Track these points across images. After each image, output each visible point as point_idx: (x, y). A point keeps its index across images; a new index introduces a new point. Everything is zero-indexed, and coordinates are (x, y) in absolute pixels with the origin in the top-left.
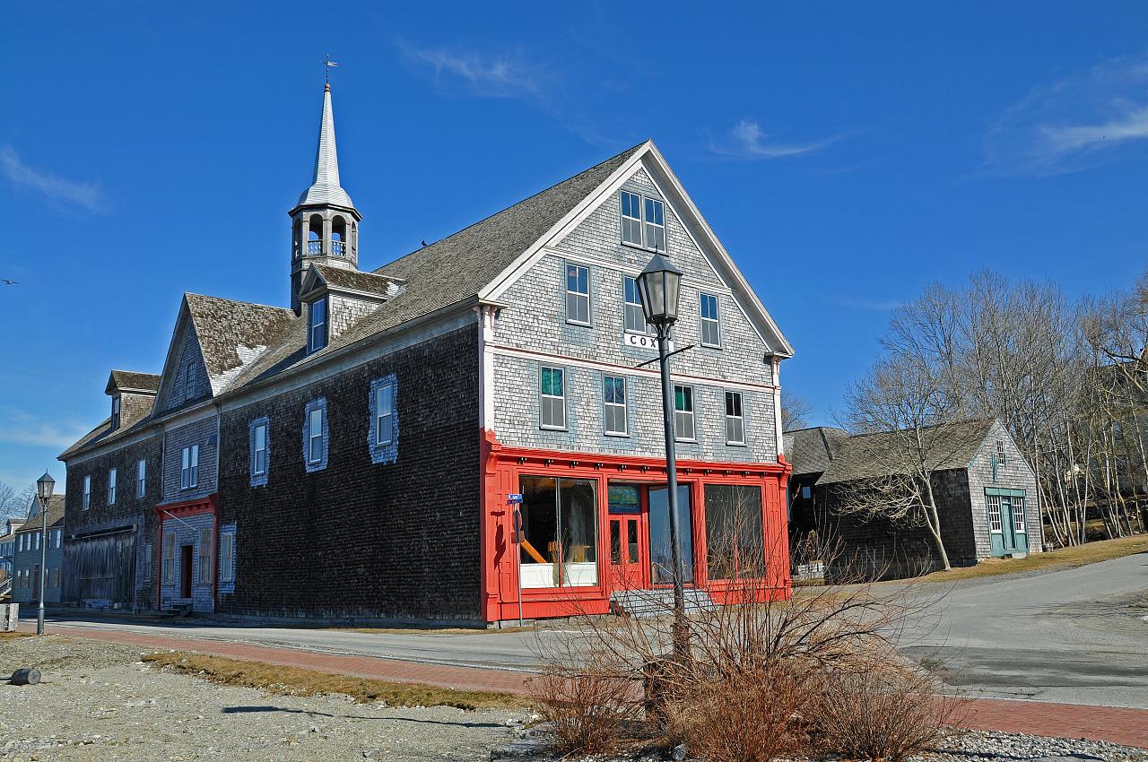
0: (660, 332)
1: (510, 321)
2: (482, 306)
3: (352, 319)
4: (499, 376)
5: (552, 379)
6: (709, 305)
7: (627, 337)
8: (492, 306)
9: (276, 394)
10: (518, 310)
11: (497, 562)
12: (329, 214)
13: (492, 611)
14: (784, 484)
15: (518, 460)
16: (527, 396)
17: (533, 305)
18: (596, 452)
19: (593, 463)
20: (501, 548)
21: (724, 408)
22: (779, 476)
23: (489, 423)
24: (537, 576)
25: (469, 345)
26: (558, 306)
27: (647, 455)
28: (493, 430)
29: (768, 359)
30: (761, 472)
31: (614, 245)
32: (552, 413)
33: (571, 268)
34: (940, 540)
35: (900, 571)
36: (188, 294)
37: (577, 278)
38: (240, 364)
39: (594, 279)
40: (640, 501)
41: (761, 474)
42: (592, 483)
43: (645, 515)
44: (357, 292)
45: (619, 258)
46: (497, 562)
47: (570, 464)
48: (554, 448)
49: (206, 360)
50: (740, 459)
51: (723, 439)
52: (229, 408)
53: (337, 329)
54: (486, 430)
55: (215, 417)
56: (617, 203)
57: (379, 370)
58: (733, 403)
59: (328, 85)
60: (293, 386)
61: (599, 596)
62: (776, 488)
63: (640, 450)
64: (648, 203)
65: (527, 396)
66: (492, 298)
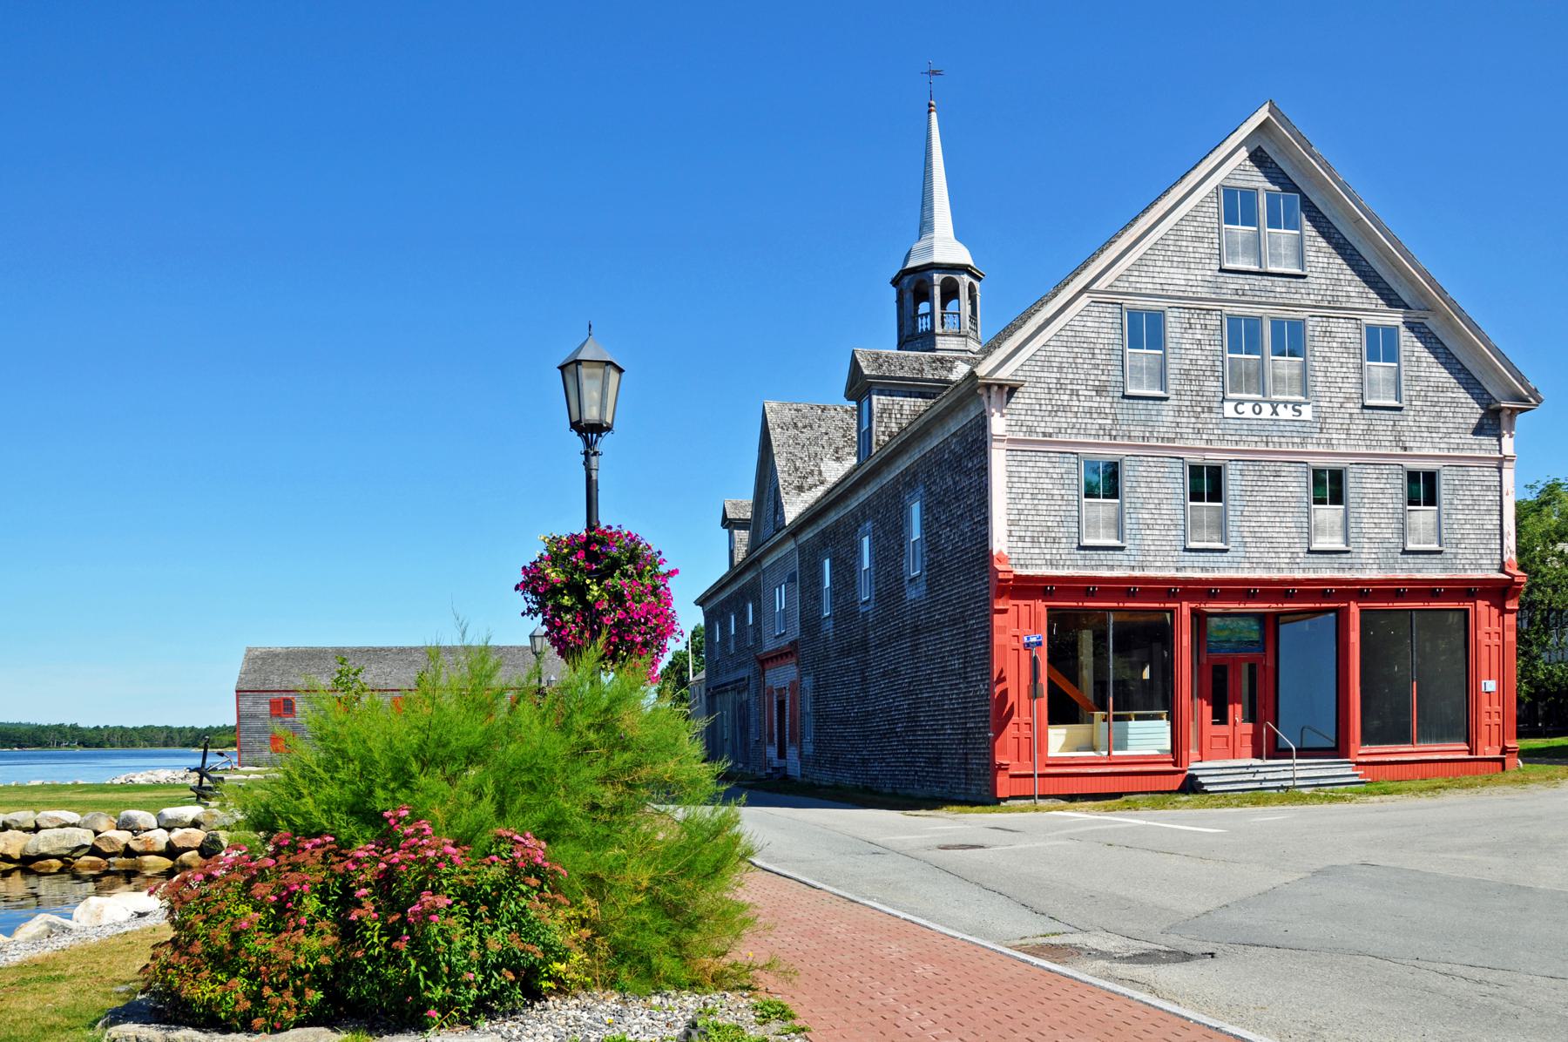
0: (589, 444)
1: (1034, 401)
2: (988, 387)
3: (904, 417)
4: (1016, 480)
8: (1001, 386)
9: (836, 518)
10: (1046, 386)
13: (1004, 785)
16: (1060, 503)
17: (1070, 376)
23: (1000, 541)
24: (1058, 740)
25: (976, 444)
28: (1006, 553)
31: (1209, 273)
33: (1134, 315)
36: (771, 405)
40: (1264, 637)
49: (781, 481)
52: (805, 537)
53: (883, 433)
54: (994, 553)
56: (1213, 209)
59: (933, 102)
60: (846, 507)
63: (1247, 565)
65: (1060, 503)
66: (1004, 374)
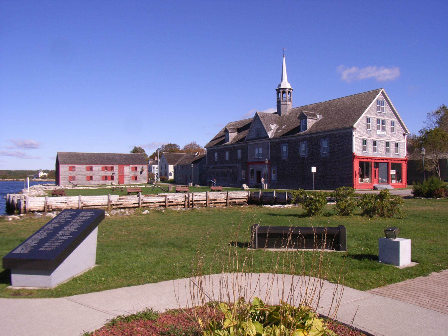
5: (364, 142)
6: (393, 124)
7: (377, 132)
11: (355, 178)
12: (287, 90)
14: (406, 163)
15: (359, 158)
18: (371, 156)
19: (371, 158)
20: (356, 176)
21: (395, 146)
22: (405, 161)
26: (365, 126)
27: (380, 157)
29: (404, 135)
30: (402, 160)
32: (364, 148)
34: (440, 176)
35: (100, 239)
37: (369, 120)
38: (272, 129)
39: (371, 120)
41: (402, 160)
42: (370, 163)
43: (378, 169)
44: (312, 118)
45: (376, 115)
46: (355, 178)
47: (367, 159)
48: (364, 156)
50: (397, 157)
51: (394, 152)
55: (268, 142)
56: (376, 102)
57: (324, 137)
58: (397, 145)
61: (371, 185)
62: (404, 163)
64: (382, 102)
